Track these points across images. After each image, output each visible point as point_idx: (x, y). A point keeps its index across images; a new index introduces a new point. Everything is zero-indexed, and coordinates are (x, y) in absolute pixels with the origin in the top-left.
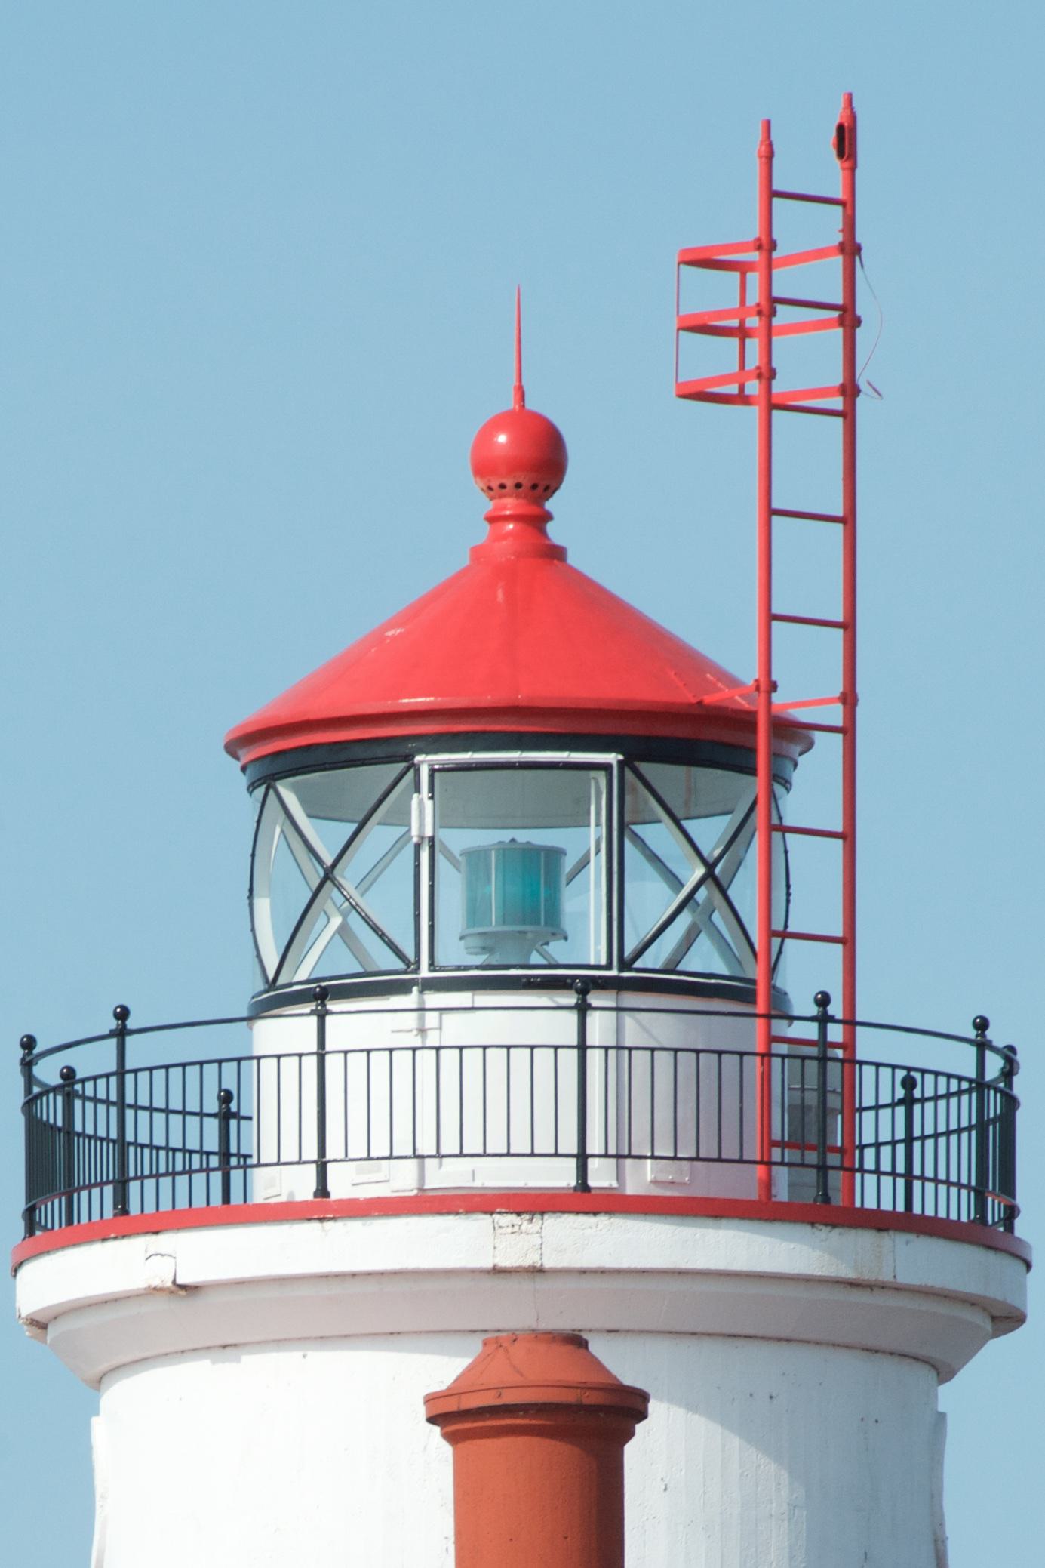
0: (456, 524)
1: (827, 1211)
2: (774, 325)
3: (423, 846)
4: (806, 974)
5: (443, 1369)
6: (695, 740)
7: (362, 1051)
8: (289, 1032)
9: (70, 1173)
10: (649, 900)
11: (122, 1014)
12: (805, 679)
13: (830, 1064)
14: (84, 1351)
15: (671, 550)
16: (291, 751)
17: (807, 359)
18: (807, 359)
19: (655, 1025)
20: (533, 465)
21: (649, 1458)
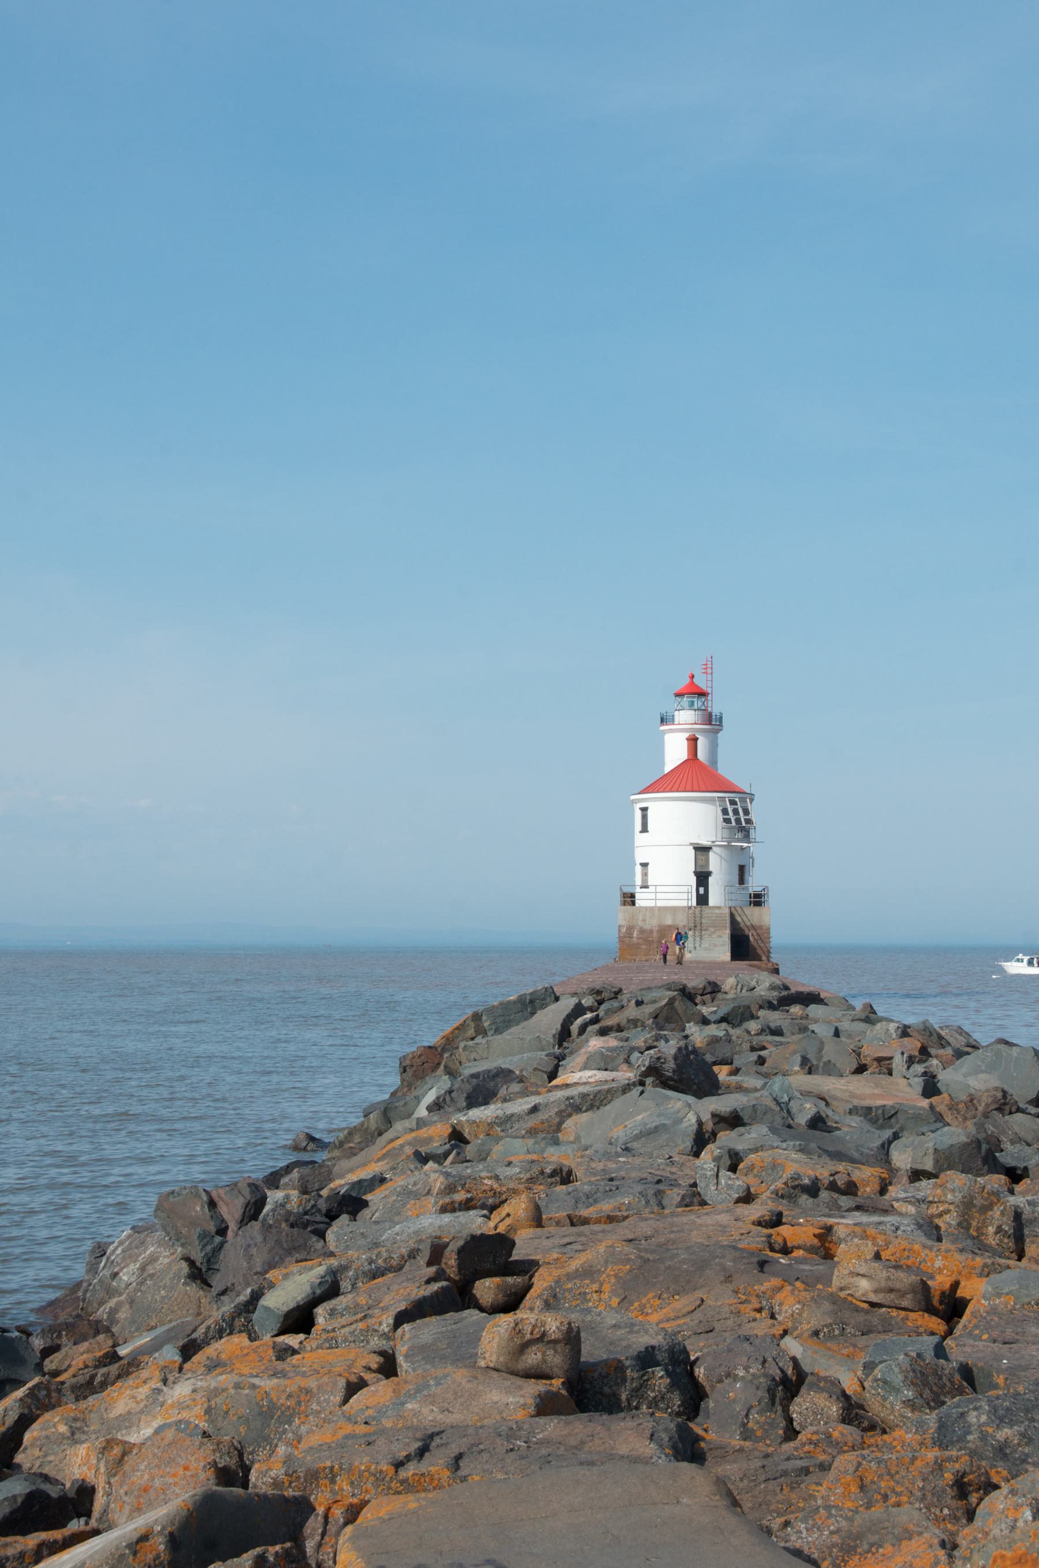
0: (688, 680)
1: (710, 724)
3: (686, 700)
4: (709, 709)
5: (687, 735)
6: (702, 694)
8: (676, 713)
9: (663, 721)
10: (700, 704)
12: (709, 690)
13: (710, 715)
14: (664, 732)
15: (701, 682)
16: (678, 695)
17: (709, 671)
18: (709, 671)
19: (700, 713)
20: (692, 677)
21: (699, 742)
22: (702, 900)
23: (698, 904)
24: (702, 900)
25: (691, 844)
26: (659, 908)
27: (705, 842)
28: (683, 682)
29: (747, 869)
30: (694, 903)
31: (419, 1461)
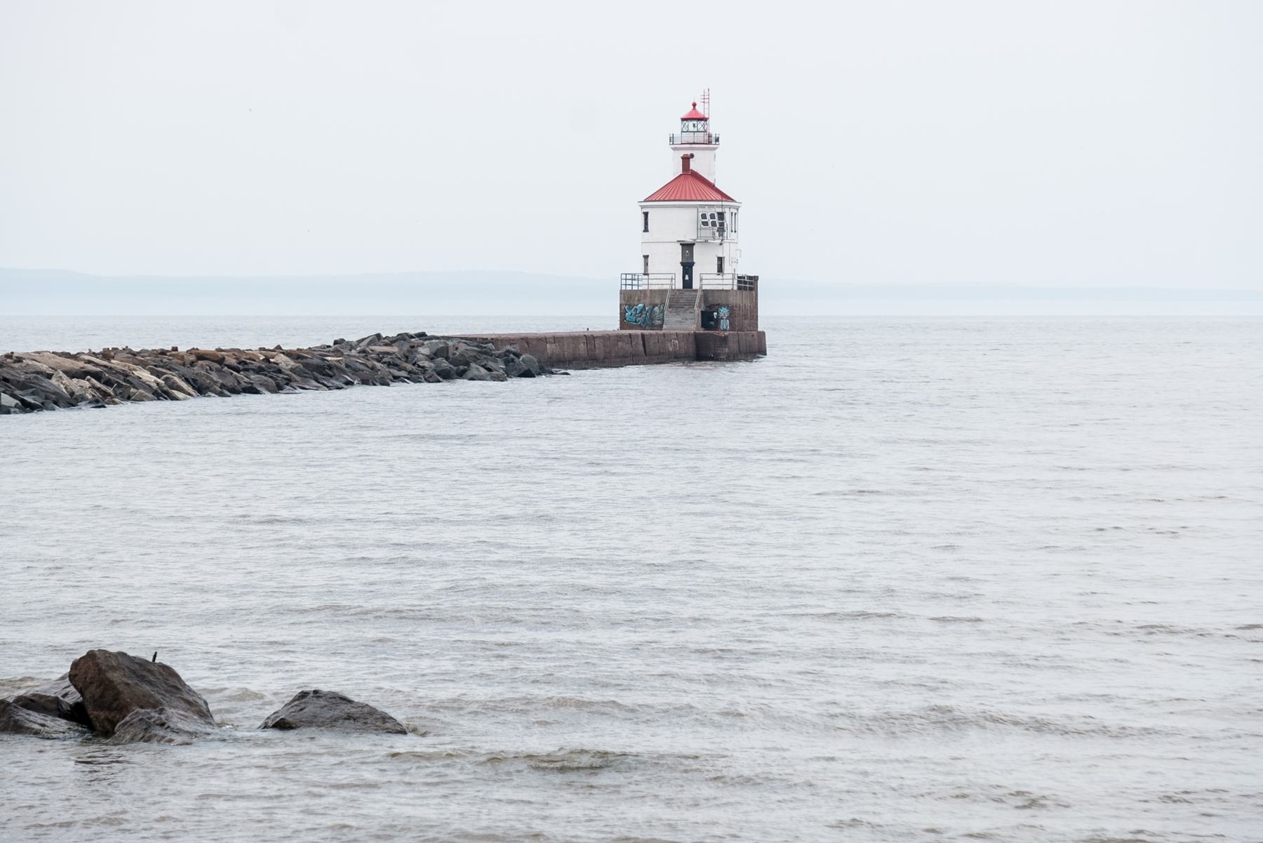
2: (706, 99)
16: (683, 120)
20: (694, 105)
22: (688, 284)
24: (688, 284)
27: (688, 239)
28: (686, 110)
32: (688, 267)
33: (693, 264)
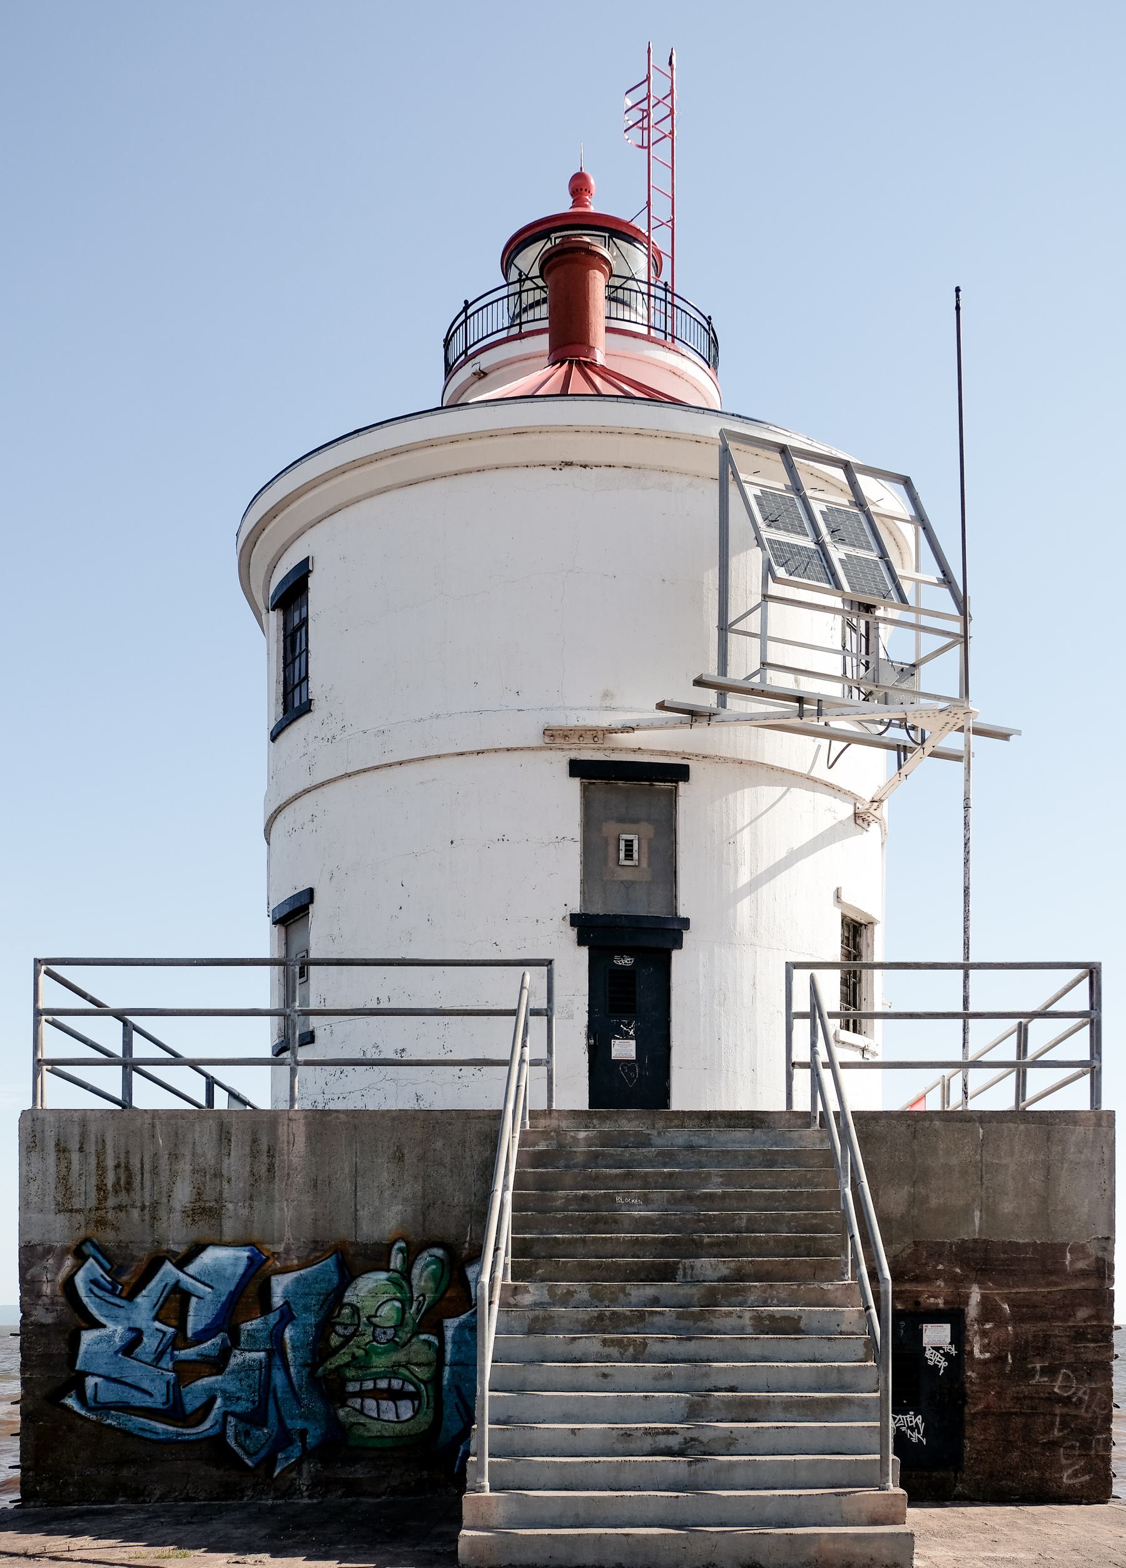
2: (651, 119)
7: (790, 1077)
11: (855, 931)
23: (597, 1096)
24: (632, 1081)
25: (554, 735)
26: (321, 1122)
29: (1099, 973)
30: (574, 1094)
31: (576, 920)
32: (631, 961)
33: (669, 932)
